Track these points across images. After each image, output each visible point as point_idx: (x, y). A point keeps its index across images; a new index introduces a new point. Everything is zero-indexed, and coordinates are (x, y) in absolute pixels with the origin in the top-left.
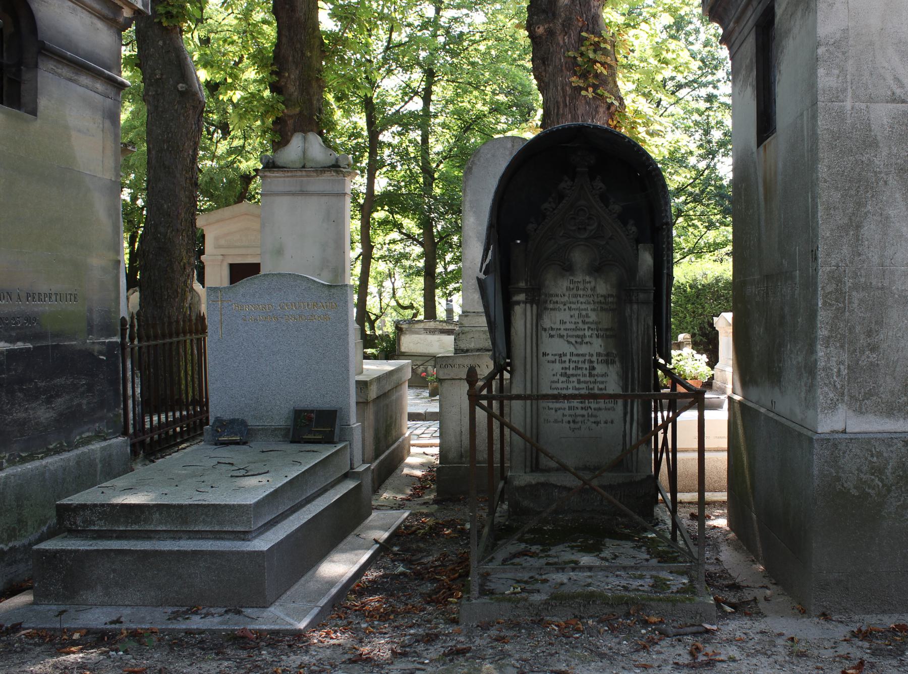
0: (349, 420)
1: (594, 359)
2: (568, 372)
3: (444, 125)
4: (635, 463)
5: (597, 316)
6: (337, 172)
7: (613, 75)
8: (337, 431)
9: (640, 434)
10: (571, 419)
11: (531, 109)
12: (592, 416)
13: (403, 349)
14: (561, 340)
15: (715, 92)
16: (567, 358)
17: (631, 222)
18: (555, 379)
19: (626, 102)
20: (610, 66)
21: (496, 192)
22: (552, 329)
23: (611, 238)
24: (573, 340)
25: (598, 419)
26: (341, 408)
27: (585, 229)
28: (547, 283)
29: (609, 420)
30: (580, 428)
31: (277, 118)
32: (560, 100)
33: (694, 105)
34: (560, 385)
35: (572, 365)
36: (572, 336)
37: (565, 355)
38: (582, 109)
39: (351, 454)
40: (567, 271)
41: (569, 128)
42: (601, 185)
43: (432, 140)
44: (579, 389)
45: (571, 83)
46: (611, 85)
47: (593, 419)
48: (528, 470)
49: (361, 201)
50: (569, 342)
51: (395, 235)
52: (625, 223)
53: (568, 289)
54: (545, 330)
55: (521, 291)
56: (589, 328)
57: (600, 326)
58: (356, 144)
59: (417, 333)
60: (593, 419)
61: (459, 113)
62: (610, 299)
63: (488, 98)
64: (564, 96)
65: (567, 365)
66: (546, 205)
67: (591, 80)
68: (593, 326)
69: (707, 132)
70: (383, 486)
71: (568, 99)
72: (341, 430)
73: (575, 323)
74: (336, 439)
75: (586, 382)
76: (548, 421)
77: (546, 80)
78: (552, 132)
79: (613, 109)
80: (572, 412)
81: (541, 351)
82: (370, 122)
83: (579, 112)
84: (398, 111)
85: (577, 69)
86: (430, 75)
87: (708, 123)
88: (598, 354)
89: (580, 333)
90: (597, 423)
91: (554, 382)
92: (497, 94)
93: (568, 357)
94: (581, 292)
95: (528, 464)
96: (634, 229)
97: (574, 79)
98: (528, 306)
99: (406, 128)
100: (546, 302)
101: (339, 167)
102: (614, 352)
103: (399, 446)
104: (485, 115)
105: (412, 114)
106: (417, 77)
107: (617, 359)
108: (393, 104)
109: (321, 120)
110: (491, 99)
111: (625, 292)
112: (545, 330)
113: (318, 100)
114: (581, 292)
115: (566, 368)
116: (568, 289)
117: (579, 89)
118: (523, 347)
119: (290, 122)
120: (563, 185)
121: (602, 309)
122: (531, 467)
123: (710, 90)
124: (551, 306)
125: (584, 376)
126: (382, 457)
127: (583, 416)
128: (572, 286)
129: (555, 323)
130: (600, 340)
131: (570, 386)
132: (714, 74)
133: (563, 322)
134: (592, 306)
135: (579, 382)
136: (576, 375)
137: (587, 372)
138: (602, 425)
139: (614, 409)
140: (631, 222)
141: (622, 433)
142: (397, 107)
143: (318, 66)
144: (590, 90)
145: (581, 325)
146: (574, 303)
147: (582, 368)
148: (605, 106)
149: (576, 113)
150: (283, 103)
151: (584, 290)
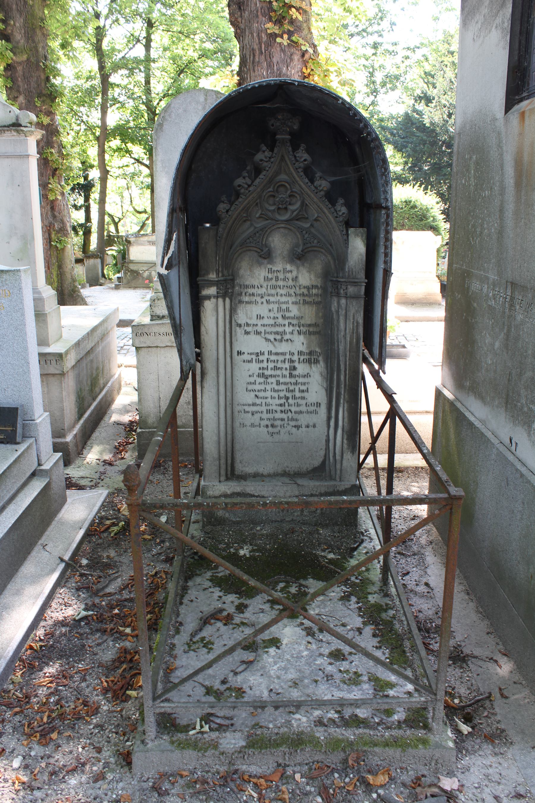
0: (33, 415)
1: (295, 358)
2: (267, 373)
3: (164, 70)
4: (338, 472)
5: (299, 310)
6: (18, 131)
7: (308, 21)
8: (19, 430)
9: (345, 441)
10: (269, 423)
11: (232, 55)
12: (292, 419)
13: (132, 258)
14: (258, 337)
15: (379, 40)
16: (264, 358)
17: (341, 201)
18: (252, 380)
20: (305, 12)
21: (178, 169)
22: (248, 325)
23: (316, 220)
24: (272, 337)
25: (299, 423)
26: (22, 406)
27: (286, 209)
28: (242, 272)
29: (311, 424)
31: (8, 65)
32: (256, 47)
35: (271, 365)
36: (271, 333)
37: (262, 354)
39: (38, 450)
40: (265, 258)
42: (306, 156)
43: (153, 81)
44: (278, 391)
45: (266, 30)
46: (306, 32)
47: (293, 423)
48: (223, 478)
50: (267, 340)
51: (127, 160)
52: (333, 203)
53: (266, 279)
54: (240, 326)
55: (211, 284)
56: (290, 324)
57: (302, 322)
59: (142, 245)
60: (293, 423)
62: (315, 291)
63: (197, 46)
64: (260, 43)
65: (265, 365)
66: (239, 181)
67: (287, 27)
68: (295, 322)
69: (372, 74)
70: (89, 443)
72: (24, 426)
74: (18, 439)
75: (285, 384)
76: (244, 425)
77: (242, 26)
79: (307, 56)
80: (270, 416)
81: (236, 349)
83: (275, 60)
85: (272, 14)
86: (150, 24)
87: (373, 67)
88: (300, 353)
89: (280, 329)
90: (298, 427)
91: (250, 383)
92: (204, 42)
93: (266, 356)
94: (281, 283)
95: (223, 472)
96: (344, 210)
97: (269, 25)
98: (220, 300)
100: (240, 295)
101: (20, 125)
102: (318, 350)
104: (195, 61)
106: (138, 27)
107: (320, 358)
108: (119, 51)
109: (46, 66)
110: (200, 47)
111: (333, 282)
112: (240, 326)
113: (43, 48)
114: (281, 283)
115: (263, 368)
116: (266, 279)
117: (274, 36)
118: (215, 347)
119: (19, 68)
120: (259, 156)
121: (305, 302)
122: (227, 475)
123: (375, 38)
124: (247, 299)
125: (284, 376)
126: (86, 415)
127: (283, 420)
130: (302, 337)
131: (268, 387)
132: (380, 24)
133: (259, 317)
134: (294, 299)
135: (278, 383)
136: (275, 376)
137: (287, 373)
138: (304, 429)
139: (316, 413)
140: (341, 201)
143: (41, 14)
144: (286, 36)
145: (280, 321)
146: (273, 295)
147: (281, 369)
148: (299, 53)
150: (11, 50)
151: (284, 280)
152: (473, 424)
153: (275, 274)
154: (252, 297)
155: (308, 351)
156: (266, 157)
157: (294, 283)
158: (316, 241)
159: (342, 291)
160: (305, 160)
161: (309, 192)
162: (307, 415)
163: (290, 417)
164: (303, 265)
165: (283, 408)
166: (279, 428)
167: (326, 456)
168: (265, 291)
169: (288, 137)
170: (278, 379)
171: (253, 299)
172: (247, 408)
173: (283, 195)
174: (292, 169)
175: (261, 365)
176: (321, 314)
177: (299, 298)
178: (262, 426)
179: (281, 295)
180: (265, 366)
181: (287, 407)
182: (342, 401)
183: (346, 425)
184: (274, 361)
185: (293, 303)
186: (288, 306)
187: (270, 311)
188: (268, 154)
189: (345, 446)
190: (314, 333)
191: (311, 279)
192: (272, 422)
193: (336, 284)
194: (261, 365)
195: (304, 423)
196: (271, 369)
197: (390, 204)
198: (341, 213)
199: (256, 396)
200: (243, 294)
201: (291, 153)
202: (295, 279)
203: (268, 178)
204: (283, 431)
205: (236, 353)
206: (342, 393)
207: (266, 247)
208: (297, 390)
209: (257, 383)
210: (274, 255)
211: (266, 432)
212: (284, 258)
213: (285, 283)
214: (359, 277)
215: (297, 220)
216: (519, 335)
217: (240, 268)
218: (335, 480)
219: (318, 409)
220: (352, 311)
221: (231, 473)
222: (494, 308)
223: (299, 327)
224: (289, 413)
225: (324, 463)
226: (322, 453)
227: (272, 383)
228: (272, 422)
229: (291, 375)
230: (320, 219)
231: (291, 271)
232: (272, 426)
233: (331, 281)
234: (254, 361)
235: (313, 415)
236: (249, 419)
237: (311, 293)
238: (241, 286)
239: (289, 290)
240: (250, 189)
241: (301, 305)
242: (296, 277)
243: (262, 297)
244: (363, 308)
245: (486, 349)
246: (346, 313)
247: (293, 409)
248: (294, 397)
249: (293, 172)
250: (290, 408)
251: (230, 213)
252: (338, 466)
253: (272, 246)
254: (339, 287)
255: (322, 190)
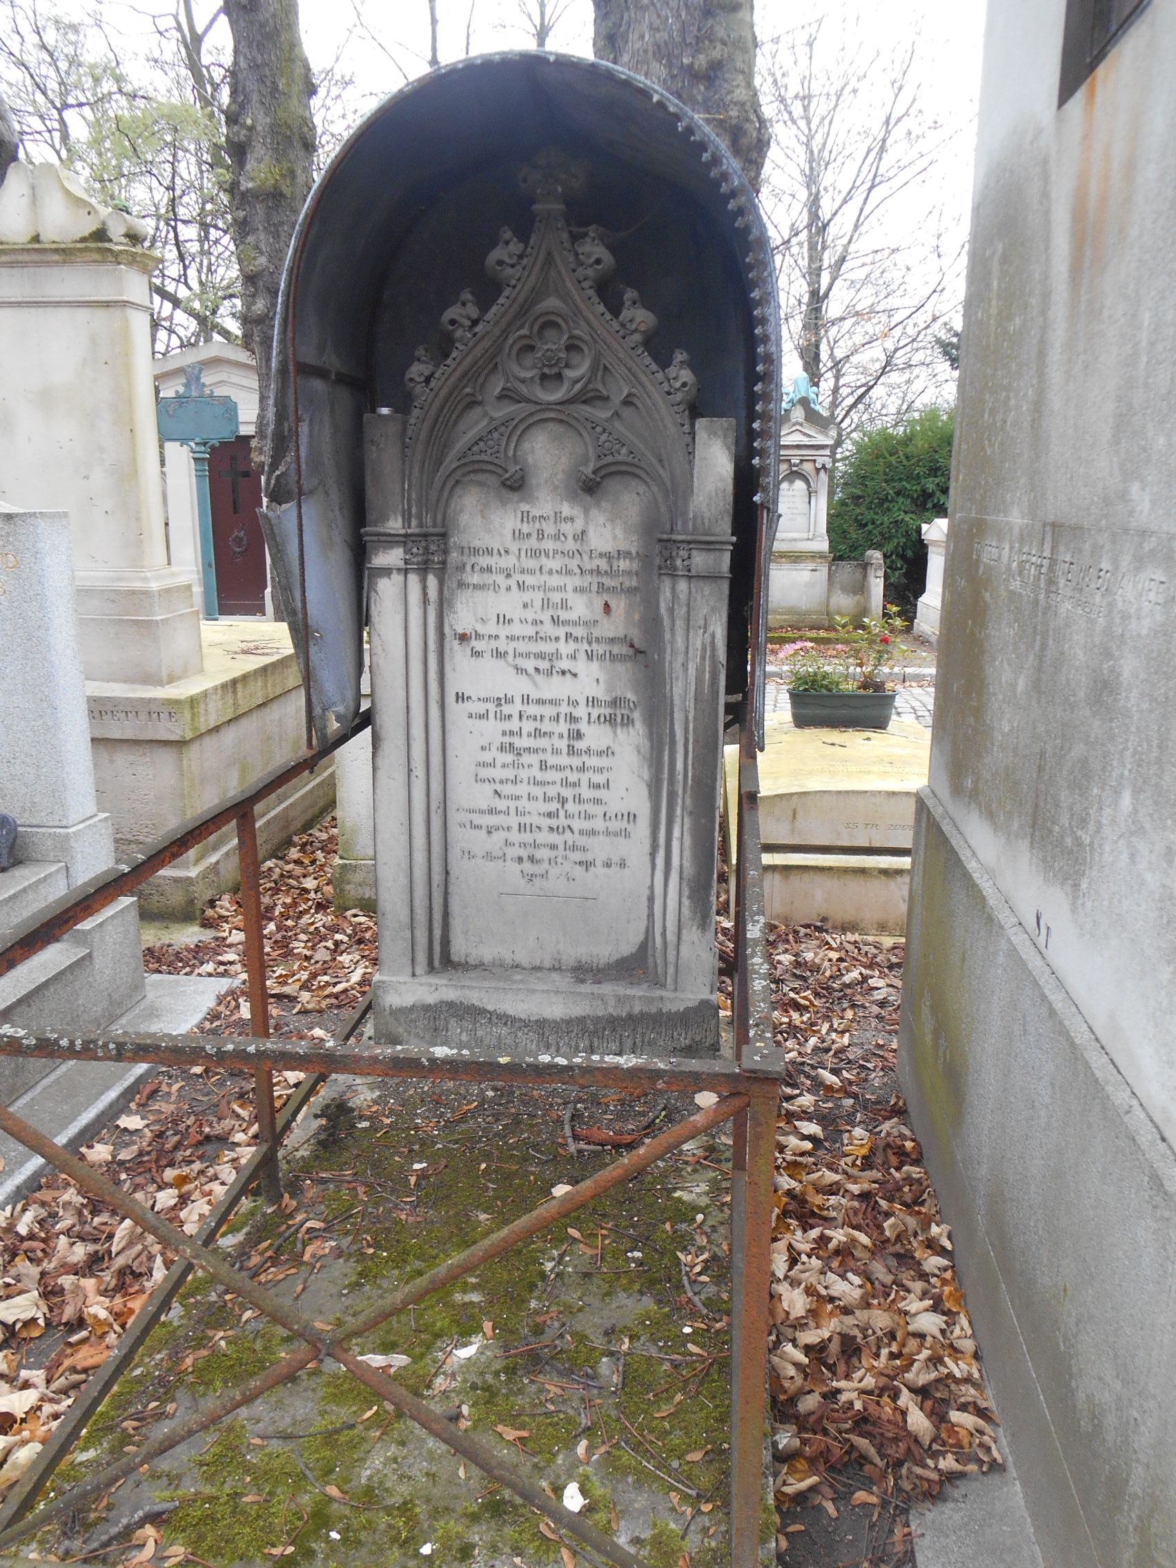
1: (581, 711)
2: (520, 743)
4: (671, 970)
9: (686, 902)
10: (524, 853)
12: (574, 848)
14: (500, 663)
16: (513, 709)
18: (487, 757)
24: (529, 665)
27: (559, 377)
28: (464, 519)
29: (616, 859)
35: (528, 726)
36: (528, 655)
37: (509, 700)
47: (577, 856)
50: (520, 670)
53: (518, 535)
55: (391, 540)
57: (597, 632)
60: (577, 856)
62: (624, 564)
65: (514, 725)
66: (453, 312)
68: (579, 632)
75: (560, 768)
76: (471, 856)
80: (527, 837)
88: (592, 702)
89: (548, 648)
90: (587, 865)
91: (484, 765)
94: (549, 545)
95: (422, 957)
96: (686, 375)
98: (413, 579)
100: (461, 568)
102: (630, 696)
107: (636, 715)
114: (549, 545)
115: (512, 733)
116: (518, 535)
124: (475, 579)
125: (556, 752)
127: (553, 847)
130: (595, 665)
131: (524, 774)
135: (543, 766)
136: (536, 751)
137: (563, 744)
138: (600, 870)
145: (548, 629)
146: (531, 572)
147: (550, 734)
151: (557, 537)
152: (971, 878)
153: (537, 525)
154: (486, 575)
155: (608, 699)
156: (510, 256)
157: (578, 546)
158: (624, 451)
159: (679, 562)
160: (598, 262)
161: (608, 337)
162: (608, 840)
163: (570, 843)
164: (598, 505)
165: (554, 822)
166: (546, 865)
167: (649, 931)
168: (515, 561)
169: (561, 207)
170: (542, 756)
171: (488, 579)
172: (477, 819)
173: (554, 343)
174: (569, 284)
175: (507, 726)
176: (637, 617)
177: (589, 578)
178: (508, 857)
179: (550, 572)
180: (516, 729)
181: (562, 821)
182: (679, 811)
183: (687, 864)
184: (535, 719)
185: (575, 590)
186: (563, 595)
187: (525, 606)
188: (515, 247)
189: (686, 911)
190: (621, 658)
191: (615, 537)
192: (531, 851)
193: (668, 545)
194: (507, 726)
195: (600, 858)
196: (529, 735)
197: (773, 349)
198: (678, 385)
199: (496, 792)
200: (468, 568)
201: (567, 245)
202: (582, 536)
203: (516, 306)
204: (554, 871)
205: (454, 698)
206: (680, 792)
207: (516, 463)
208: (585, 784)
209: (498, 764)
210: (534, 482)
211: (518, 872)
212: (556, 488)
213: (558, 546)
214: (718, 530)
215: (585, 402)
216: (1062, 654)
217: (462, 510)
218: (663, 986)
219: (630, 827)
220: (702, 610)
221: (443, 960)
222: (1020, 595)
223: (590, 643)
224: (568, 831)
225: (644, 947)
226: (643, 925)
227: (530, 766)
228: (531, 851)
229: (572, 751)
230: (635, 400)
231: (572, 519)
232: (532, 859)
233: (660, 540)
234: (491, 715)
235: (621, 840)
236: (479, 842)
237: (615, 568)
238: (462, 550)
239: (567, 561)
240: (477, 329)
241: (594, 595)
242: (583, 532)
243: (508, 576)
244: (726, 601)
245: (1001, 697)
246: (688, 612)
247: (577, 824)
248: (578, 799)
249: (573, 290)
250: (569, 822)
251: (432, 384)
252: (671, 956)
253: (530, 460)
254: (674, 554)
255: (636, 330)
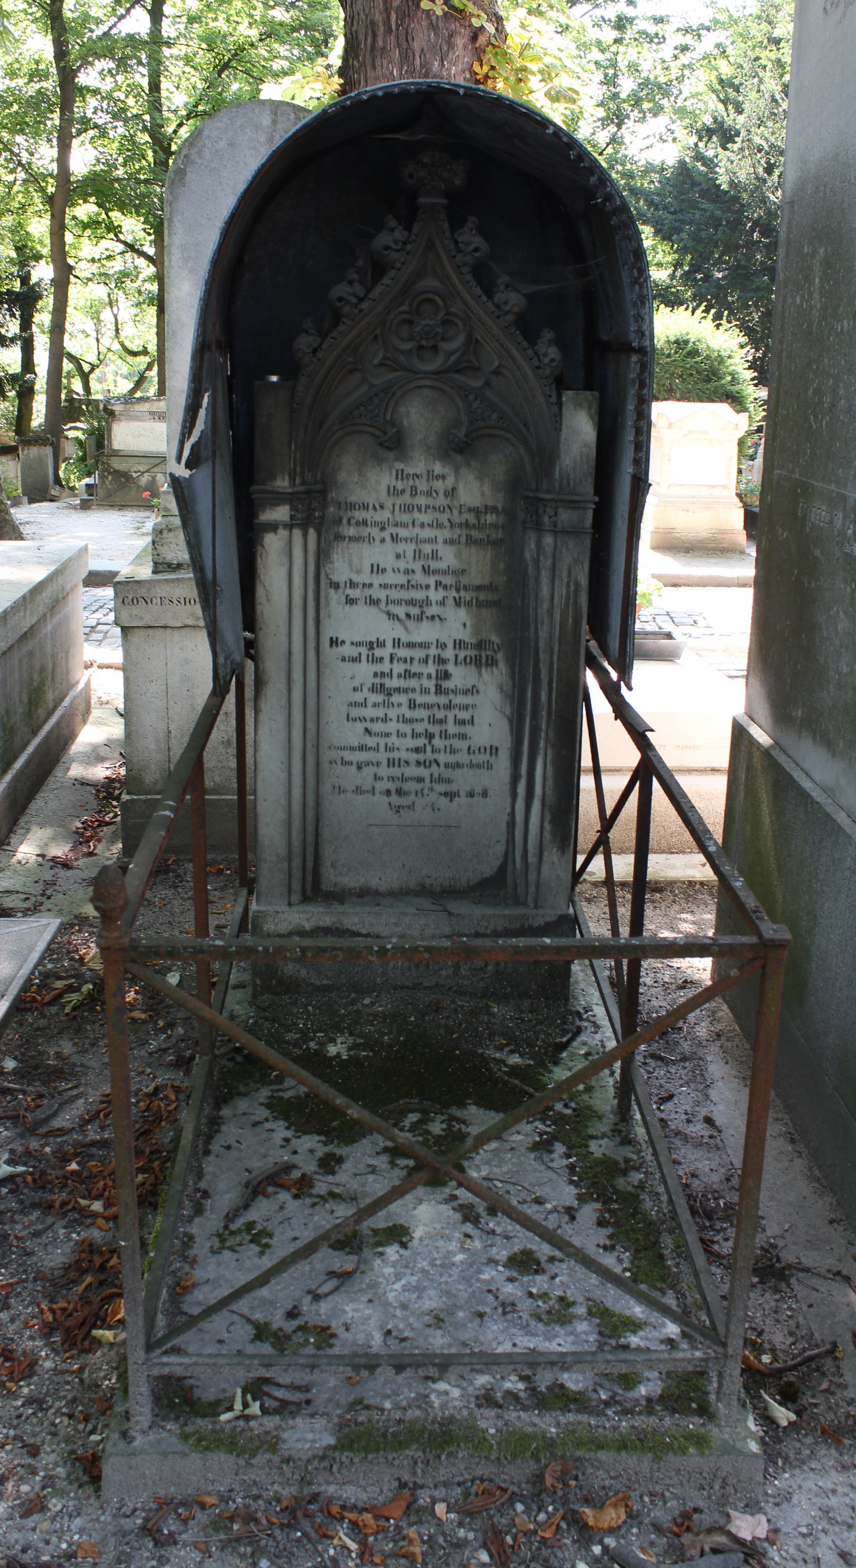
1: (449, 653)
2: (390, 683)
3: (188, 60)
4: (532, 888)
5: (458, 556)
9: (547, 826)
10: (392, 786)
11: (328, 36)
12: (441, 780)
13: (116, 446)
14: (373, 610)
15: (630, 12)
16: (384, 653)
17: (548, 335)
18: (359, 697)
19: (508, 26)
22: (353, 584)
23: (496, 373)
24: (401, 611)
25: (454, 787)
27: (435, 348)
28: (342, 476)
29: (478, 790)
30: (412, 807)
32: (378, 18)
33: (593, 34)
34: (369, 712)
35: (399, 668)
36: (399, 602)
37: (381, 644)
38: (421, 39)
40: (389, 449)
41: (404, 94)
42: (478, 241)
43: (165, 84)
44: (411, 721)
47: (441, 788)
48: (296, 898)
49: (51, 190)
50: (391, 616)
53: (393, 492)
54: (336, 586)
55: (278, 499)
56: (438, 584)
57: (464, 580)
58: (39, 92)
60: (441, 788)
61: (211, 41)
62: (490, 518)
63: (257, 15)
64: (387, 11)
65: (386, 667)
66: (340, 290)
68: (448, 580)
70: (22, 821)
71: (393, 16)
73: (407, 572)
75: (427, 706)
76: (340, 790)
78: (359, 105)
79: (482, 40)
80: (396, 772)
81: (328, 632)
82: (61, 54)
83: (416, 46)
84: (106, 34)
88: (459, 644)
89: (419, 595)
90: (451, 796)
91: (356, 704)
92: (273, 8)
93: (389, 649)
94: (422, 501)
95: (296, 886)
96: (553, 353)
98: (297, 534)
99: (122, 64)
100: (338, 522)
102: (494, 638)
103: (58, 723)
105: (132, 40)
107: (500, 656)
108: (98, 22)
110: (263, 16)
111: (527, 500)
112: (336, 586)
114: (422, 501)
115: (383, 674)
116: (393, 492)
118: (283, 630)
120: (383, 239)
121: (471, 541)
122: (304, 891)
124: (351, 531)
125: (425, 691)
127: (420, 780)
128: (400, 485)
129: (359, 572)
130: (462, 612)
131: (392, 713)
133: (377, 569)
134: (447, 534)
135: (412, 705)
136: (406, 691)
137: (431, 685)
138: (463, 800)
139: (489, 767)
140: (548, 335)
141: (505, 818)
142: (104, 28)
145: (419, 577)
146: (405, 525)
147: (419, 675)
148: (466, 33)
149: (409, 47)
151: (429, 494)
